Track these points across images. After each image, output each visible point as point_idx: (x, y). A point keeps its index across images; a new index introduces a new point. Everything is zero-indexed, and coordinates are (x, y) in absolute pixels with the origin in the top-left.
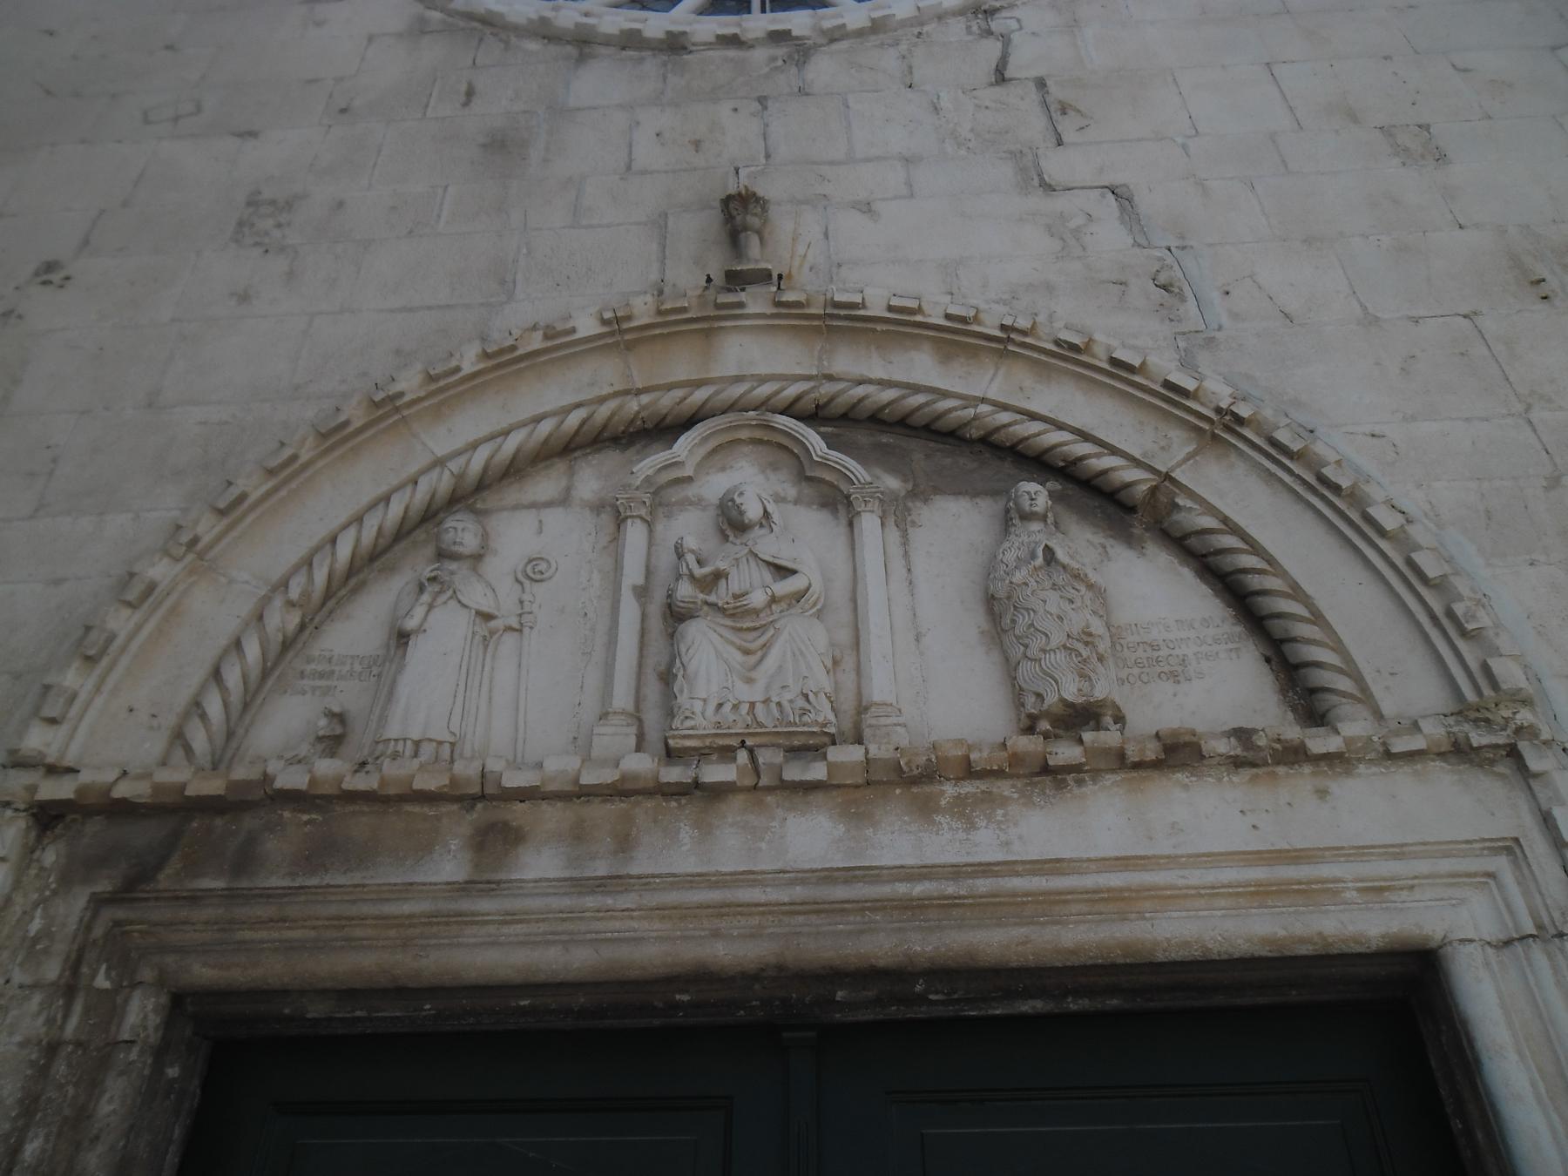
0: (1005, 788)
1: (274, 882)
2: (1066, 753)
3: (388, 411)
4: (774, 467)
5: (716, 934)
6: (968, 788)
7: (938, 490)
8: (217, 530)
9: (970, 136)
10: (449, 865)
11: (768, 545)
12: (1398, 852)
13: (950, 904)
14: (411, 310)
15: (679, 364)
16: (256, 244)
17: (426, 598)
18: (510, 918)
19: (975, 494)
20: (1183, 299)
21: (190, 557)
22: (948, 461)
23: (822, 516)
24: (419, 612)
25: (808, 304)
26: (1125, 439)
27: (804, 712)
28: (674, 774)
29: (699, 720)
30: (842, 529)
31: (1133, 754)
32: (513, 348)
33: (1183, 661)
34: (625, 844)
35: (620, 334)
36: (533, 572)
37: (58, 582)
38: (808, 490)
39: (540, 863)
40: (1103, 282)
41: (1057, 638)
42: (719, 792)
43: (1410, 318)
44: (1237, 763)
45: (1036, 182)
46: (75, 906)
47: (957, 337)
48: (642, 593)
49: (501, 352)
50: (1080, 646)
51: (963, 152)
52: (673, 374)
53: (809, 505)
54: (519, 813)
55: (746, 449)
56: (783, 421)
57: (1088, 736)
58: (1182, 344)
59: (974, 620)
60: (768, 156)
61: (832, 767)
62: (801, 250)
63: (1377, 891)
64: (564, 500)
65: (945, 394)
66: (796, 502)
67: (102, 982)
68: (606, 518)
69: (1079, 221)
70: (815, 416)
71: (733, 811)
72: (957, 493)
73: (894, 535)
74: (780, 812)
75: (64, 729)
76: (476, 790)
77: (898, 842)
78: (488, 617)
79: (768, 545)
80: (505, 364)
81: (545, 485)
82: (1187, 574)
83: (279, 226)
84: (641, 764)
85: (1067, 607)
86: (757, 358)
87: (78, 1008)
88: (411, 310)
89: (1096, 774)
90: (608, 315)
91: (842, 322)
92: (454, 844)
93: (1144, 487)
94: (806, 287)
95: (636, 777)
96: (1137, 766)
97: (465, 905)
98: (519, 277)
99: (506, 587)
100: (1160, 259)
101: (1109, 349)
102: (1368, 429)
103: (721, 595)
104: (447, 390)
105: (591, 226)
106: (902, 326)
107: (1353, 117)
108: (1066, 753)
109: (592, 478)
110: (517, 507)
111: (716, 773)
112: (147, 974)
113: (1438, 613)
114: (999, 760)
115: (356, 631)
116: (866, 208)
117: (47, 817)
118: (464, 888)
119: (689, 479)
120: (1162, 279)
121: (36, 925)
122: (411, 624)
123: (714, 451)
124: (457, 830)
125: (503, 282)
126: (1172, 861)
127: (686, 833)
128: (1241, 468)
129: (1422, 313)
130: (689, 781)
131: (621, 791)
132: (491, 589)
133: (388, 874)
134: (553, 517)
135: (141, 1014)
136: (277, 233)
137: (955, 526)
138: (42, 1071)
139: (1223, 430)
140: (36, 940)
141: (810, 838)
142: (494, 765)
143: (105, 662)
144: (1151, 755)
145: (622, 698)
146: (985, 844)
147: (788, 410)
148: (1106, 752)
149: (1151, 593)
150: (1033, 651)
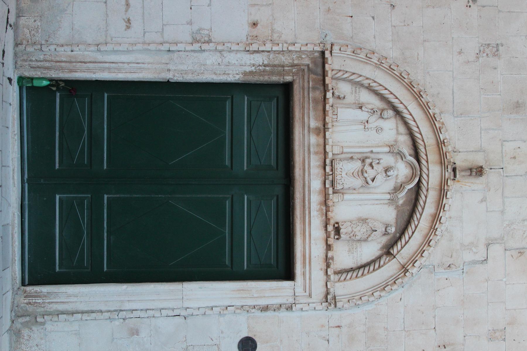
0: (324, 217)
1: (311, 95)
2: (330, 228)
3: (418, 96)
4: (406, 177)
5: (300, 169)
6: (324, 211)
7: (398, 211)
8: (386, 67)
9: (512, 228)
10: (313, 124)
11: (380, 178)
12: (310, 279)
13: (304, 206)
14: (453, 94)
15: (433, 157)
16: (480, 51)
17: (370, 111)
18: (304, 135)
19: (397, 219)
20: (445, 269)
21: (379, 63)
22: (407, 214)
23: (392, 188)
24: (366, 110)
25: (447, 186)
26: (405, 251)
27: (339, 184)
28: (328, 162)
29: (338, 165)
30: (388, 192)
31: (329, 239)
32: (436, 120)
33: (353, 253)
34: (316, 153)
35: (440, 144)
36: (379, 130)
37: (375, 37)
38: (399, 185)
39: (314, 139)
40: (452, 253)
41: (355, 230)
42: (325, 169)
43: (435, 316)
44: (327, 256)
45: (490, 242)
46: (307, 61)
47: (436, 218)
48: (372, 152)
49: (435, 118)
50: (353, 233)
51: (505, 225)
52: (430, 154)
53: (395, 185)
54: (322, 134)
55: (412, 171)
56: (417, 180)
57: (333, 232)
58: (431, 266)
59: (364, 217)
60: (507, 176)
61: (328, 188)
62: (469, 184)
63: (304, 274)
64: (398, 133)
65: (421, 215)
66: (396, 182)
67: (294, 70)
68: (393, 143)
69: (474, 250)
70: (419, 185)
71: (322, 171)
72: (397, 215)
73: (386, 202)
74: (321, 179)
75: (339, 52)
76: (326, 127)
77: (315, 199)
78: (367, 122)
79: (380, 178)
80: (432, 119)
81: (402, 129)
82: (373, 258)
83: (487, 55)
84: (330, 155)
85: (362, 233)
86: (433, 174)
87: (290, 68)
88: (453, 94)
89: (326, 233)
90: (445, 141)
91: (442, 193)
92: (317, 124)
93: (392, 252)
94: (453, 187)
95: (328, 155)
96: (327, 240)
97: (306, 128)
98: (463, 118)
99: (376, 124)
100: (459, 267)
101: (428, 250)
102: (403, 298)
103: (367, 168)
104: (425, 108)
105: (481, 133)
106: (440, 206)
107: (510, 324)
108: (330, 228)
109: (404, 140)
110: (397, 124)
111: (328, 169)
112: (295, 78)
113: (357, 300)
114: (329, 217)
115: (366, 97)
116: (483, 200)
117: (323, 53)
118: (309, 127)
119: (402, 160)
120: (451, 266)
121: (303, 56)
122: (363, 108)
123: (409, 164)
124: (320, 124)
125: (461, 114)
126: (310, 243)
127: (318, 163)
128: (395, 272)
129: (436, 319)
130: (327, 165)
131: (325, 153)
132: (375, 122)
133: (312, 114)
134: (394, 132)
135: (288, 78)
136: (485, 55)
137: (389, 215)
138: (279, 66)
139: (404, 269)
140: (301, 57)
141: (316, 184)
142: (330, 130)
143: (354, 55)
144: (328, 242)
145: (345, 150)
146: (314, 213)
147: (420, 181)
148: (330, 235)
149: (370, 250)
150: (352, 225)
